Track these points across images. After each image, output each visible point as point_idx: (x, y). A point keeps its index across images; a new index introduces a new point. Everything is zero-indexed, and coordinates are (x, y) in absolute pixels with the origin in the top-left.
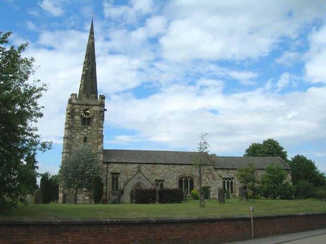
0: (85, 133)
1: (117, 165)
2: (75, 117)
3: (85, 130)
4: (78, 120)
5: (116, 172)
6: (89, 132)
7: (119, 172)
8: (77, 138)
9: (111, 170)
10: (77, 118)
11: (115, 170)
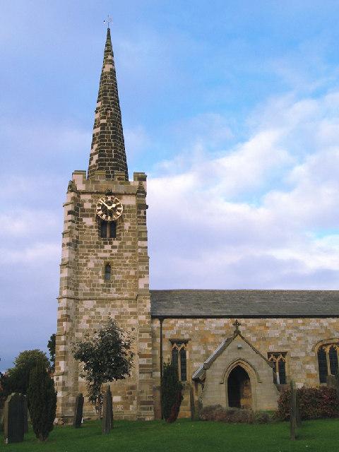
0: (108, 255)
1: (181, 322)
2: (85, 220)
3: (108, 247)
4: (92, 227)
5: (181, 338)
6: (115, 251)
7: (187, 337)
8: (91, 265)
9: (169, 334)
10: (89, 221)
11: (178, 332)
